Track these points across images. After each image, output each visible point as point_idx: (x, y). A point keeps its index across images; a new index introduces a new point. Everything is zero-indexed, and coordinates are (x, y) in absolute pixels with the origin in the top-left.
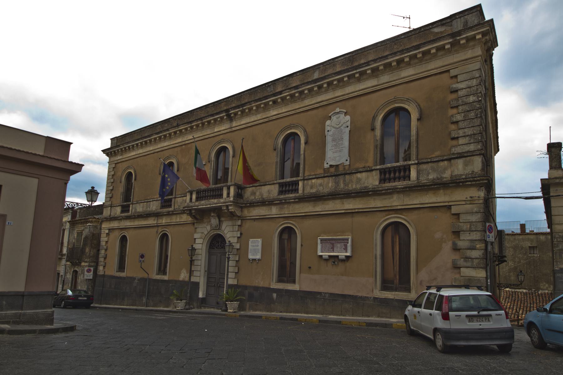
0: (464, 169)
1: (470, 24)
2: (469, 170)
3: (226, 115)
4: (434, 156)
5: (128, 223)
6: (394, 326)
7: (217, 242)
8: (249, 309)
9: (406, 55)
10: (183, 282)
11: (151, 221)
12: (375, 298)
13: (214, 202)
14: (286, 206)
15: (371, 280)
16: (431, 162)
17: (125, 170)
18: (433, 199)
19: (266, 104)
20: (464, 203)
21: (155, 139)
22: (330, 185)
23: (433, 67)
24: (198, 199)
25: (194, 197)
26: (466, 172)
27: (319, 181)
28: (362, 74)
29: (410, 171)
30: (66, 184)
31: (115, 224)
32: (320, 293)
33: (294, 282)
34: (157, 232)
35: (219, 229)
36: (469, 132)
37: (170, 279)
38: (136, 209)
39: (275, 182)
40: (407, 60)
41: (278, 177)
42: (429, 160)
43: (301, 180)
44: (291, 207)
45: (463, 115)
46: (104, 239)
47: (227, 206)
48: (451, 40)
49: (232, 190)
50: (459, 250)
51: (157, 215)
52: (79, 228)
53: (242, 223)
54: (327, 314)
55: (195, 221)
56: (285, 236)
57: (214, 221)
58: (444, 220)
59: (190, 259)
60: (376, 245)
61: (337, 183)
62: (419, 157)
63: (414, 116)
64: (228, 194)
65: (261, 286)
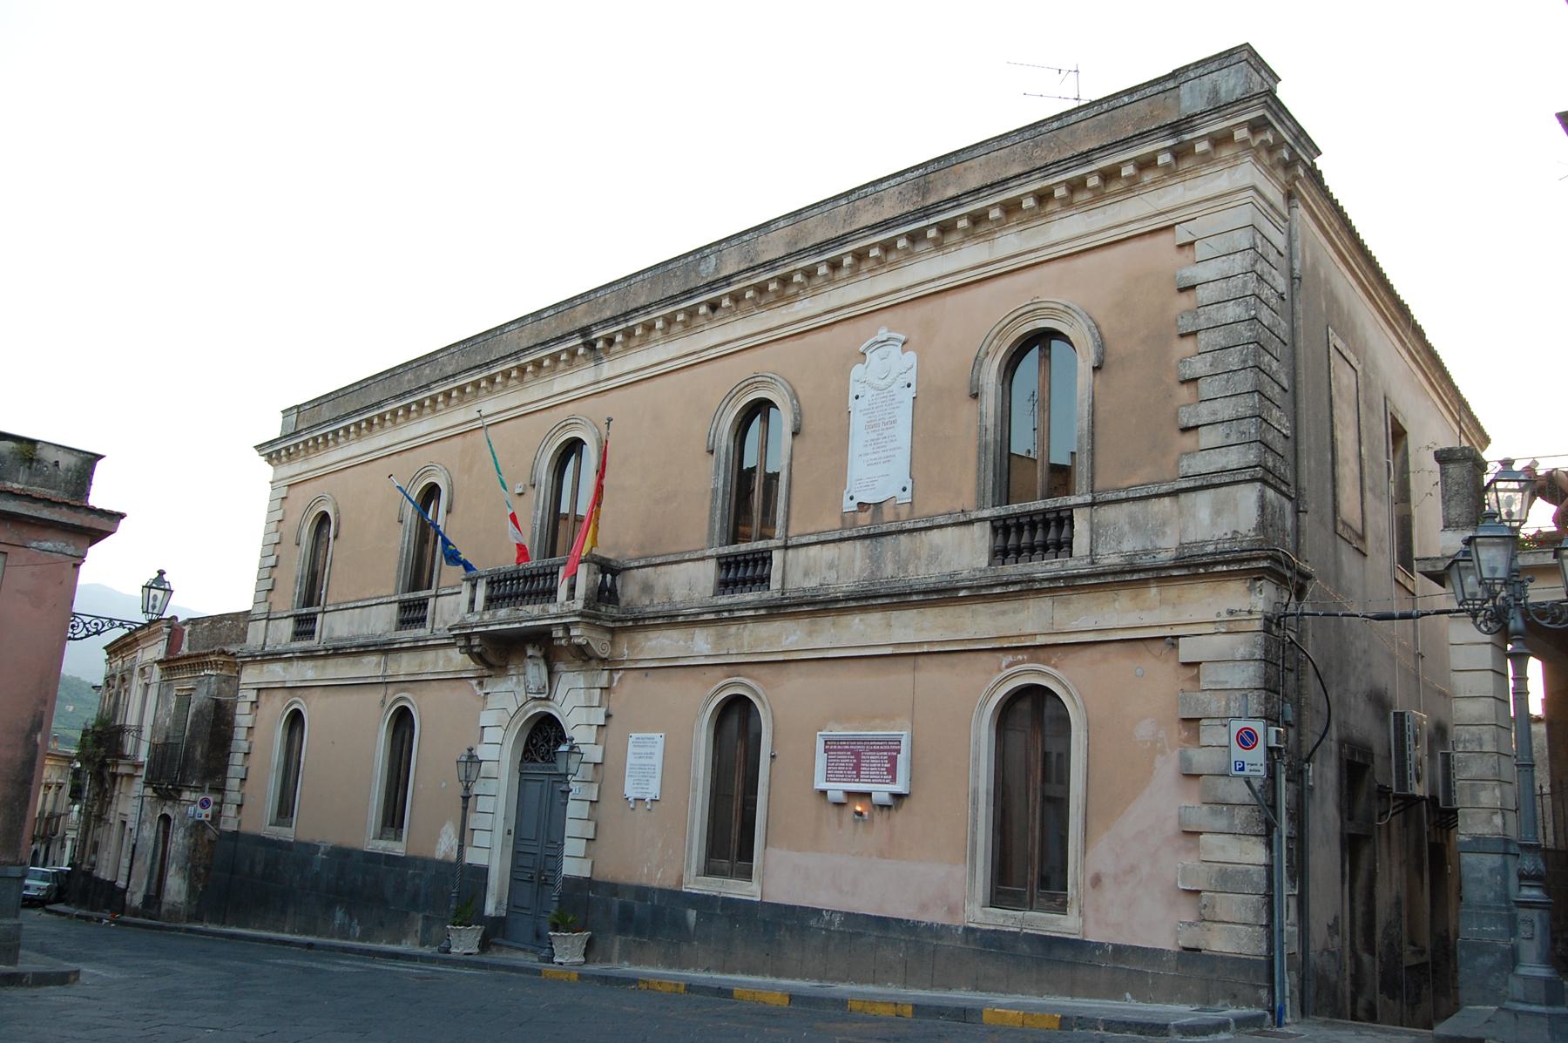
0: (1214, 524)
1: (1224, 97)
2: (1223, 530)
3: (584, 344)
4: (1135, 481)
5: (307, 672)
6: (986, 1017)
7: (543, 736)
8: (621, 960)
9: (1057, 179)
10: (444, 865)
11: (369, 667)
12: (968, 930)
13: (531, 615)
14: (733, 629)
15: (961, 871)
16: (1127, 500)
17: (310, 507)
18: (1132, 619)
19: (692, 313)
20: (1210, 629)
21: (394, 413)
22: (858, 564)
23: (1132, 216)
24: (491, 602)
25: (481, 593)
26: (1219, 534)
27: (829, 552)
28: (946, 228)
29: (1072, 526)
30: (77, 566)
31: (276, 673)
32: (817, 912)
33: (747, 875)
34: (383, 702)
35: (547, 699)
36: (1225, 409)
37: (411, 853)
38: (331, 630)
39: (708, 553)
40: (1060, 192)
41: (989, 494)
42: (1123, 495)
43: (778, 548)
44: (747, 632)
45: (1209, 357)
46: (243, 717)
47: (567, 627)
48: (1170, 143)
49: (582, 571)
50: (1199, 776)
51: (384, 649)
52: (184, 681)
53: (611, 680)
54: (834, 980)
55: (486, 672)
56: (734, 723)
57: (535, 673)
58: (1155, 679)
59: (461, 792)
60: (977, 759)
61: (876, 560)
62: (1098, 485)
63: (1085, 360)
64: (572, 588)
65: (655, 884)
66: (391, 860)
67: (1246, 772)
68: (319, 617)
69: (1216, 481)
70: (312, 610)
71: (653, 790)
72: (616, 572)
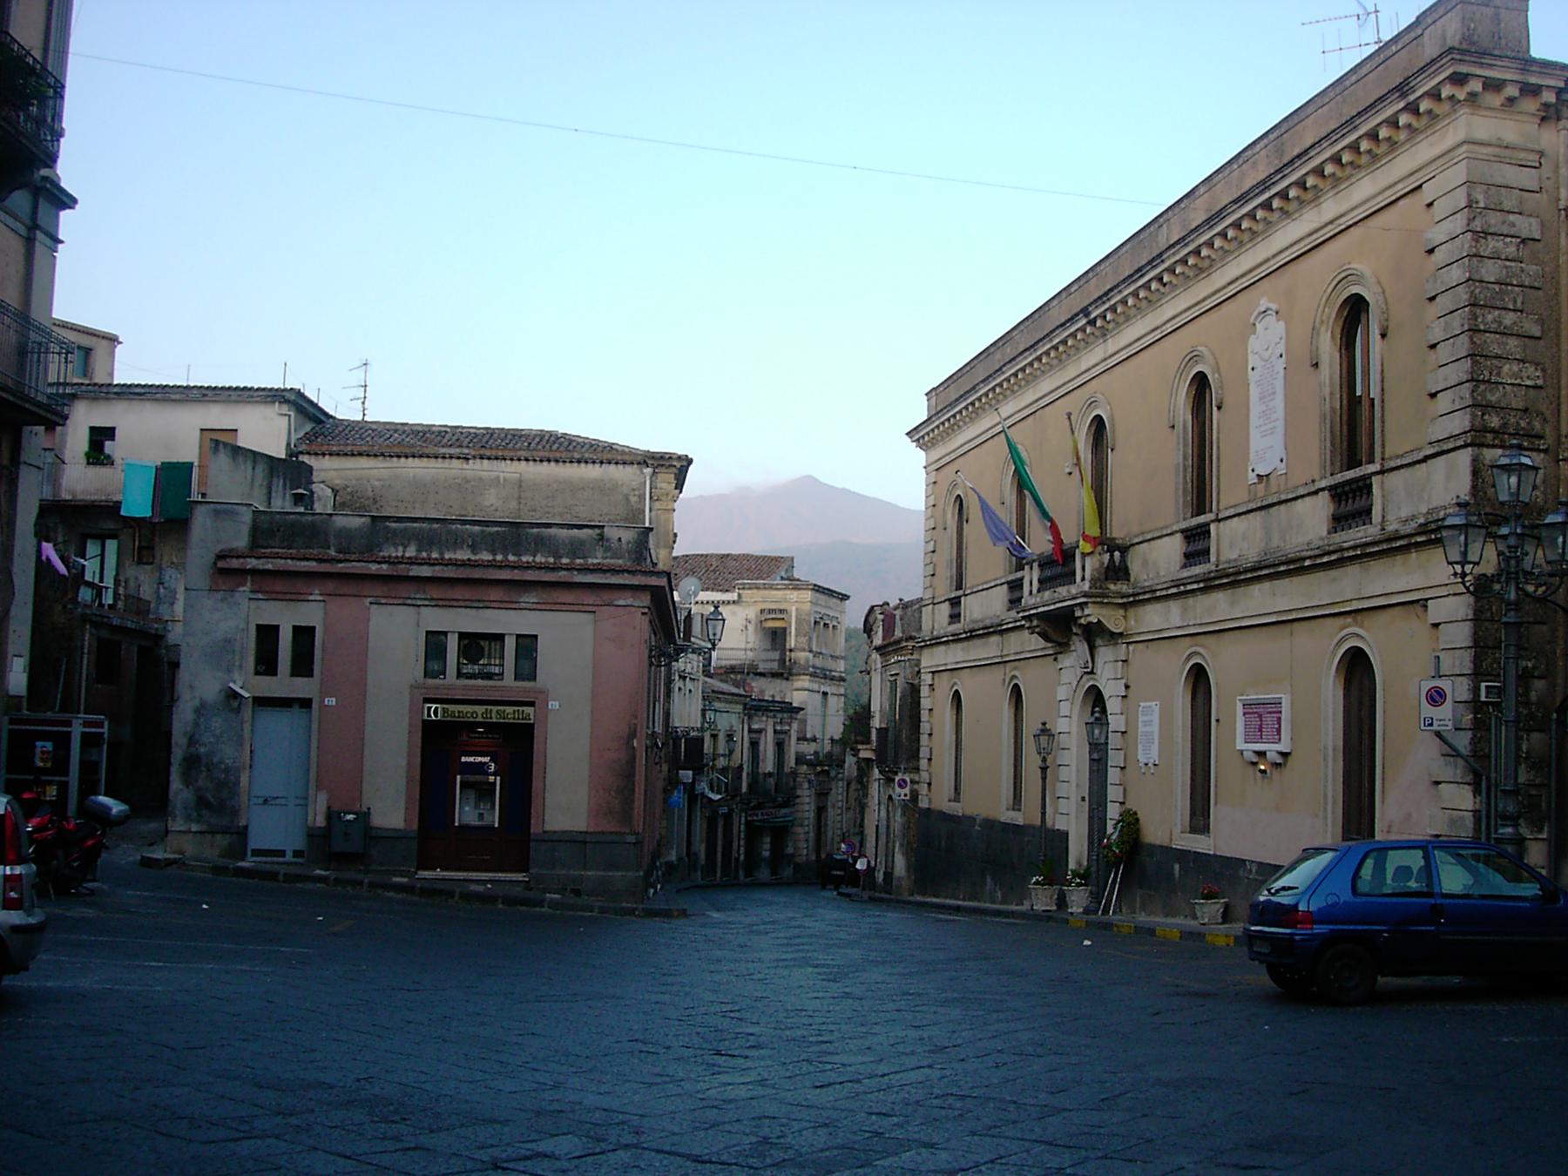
5: (1219, 607)
48: (1402, 105)
66: (1015, 828)
67: (1435, 727)
68: (1213, 527)
69: (1445, 447)
70: (1202, 519)
71: (1154, 756)
72: (1124, 550)
